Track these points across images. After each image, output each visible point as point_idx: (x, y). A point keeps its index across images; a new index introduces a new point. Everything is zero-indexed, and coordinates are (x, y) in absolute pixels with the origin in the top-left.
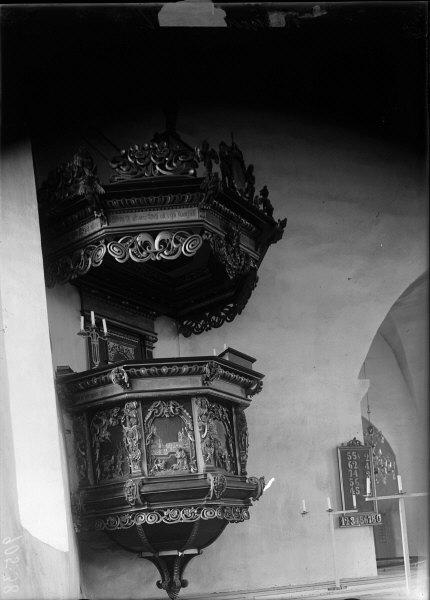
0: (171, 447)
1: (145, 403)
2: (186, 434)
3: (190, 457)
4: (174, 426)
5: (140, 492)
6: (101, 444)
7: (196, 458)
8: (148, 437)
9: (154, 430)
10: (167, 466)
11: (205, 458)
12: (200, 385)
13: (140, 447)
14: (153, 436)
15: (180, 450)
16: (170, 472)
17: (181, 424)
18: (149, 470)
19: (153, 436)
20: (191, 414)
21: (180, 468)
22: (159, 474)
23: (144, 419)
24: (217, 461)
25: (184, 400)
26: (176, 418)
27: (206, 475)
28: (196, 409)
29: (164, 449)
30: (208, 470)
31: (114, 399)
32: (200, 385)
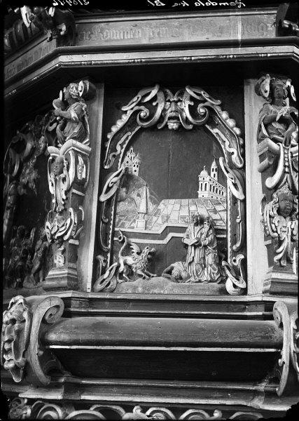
0: (175, 211)
1: (117, 83)
2: (222, 179)
3: (225, 246)
4: (183, 159)
5: (43, 342)
6: (19, 199)
7: (243, 248)
8: (112, 179)
9: (132, 162)
10: (156, 263)
11: (271, 251)
12: (272, 35)
13: (80, 201)
14: (127, 179)
15: (200, 221)
16: (162, 287)
17: (211, 150)
18: (97, 271)
19: (127, 179)
20: (240, 124)
21: (195, 276)
22: (128, 289)
23: (106, 129)
24: (166, 92)
25: (225, 79)
26: (197, 143)
27: (269, 306)
28: (254, 109)
29: (148, 217)
30: (277, 289)
31: (34, 76)
32: (272, 35)
